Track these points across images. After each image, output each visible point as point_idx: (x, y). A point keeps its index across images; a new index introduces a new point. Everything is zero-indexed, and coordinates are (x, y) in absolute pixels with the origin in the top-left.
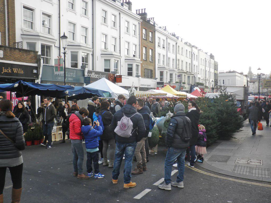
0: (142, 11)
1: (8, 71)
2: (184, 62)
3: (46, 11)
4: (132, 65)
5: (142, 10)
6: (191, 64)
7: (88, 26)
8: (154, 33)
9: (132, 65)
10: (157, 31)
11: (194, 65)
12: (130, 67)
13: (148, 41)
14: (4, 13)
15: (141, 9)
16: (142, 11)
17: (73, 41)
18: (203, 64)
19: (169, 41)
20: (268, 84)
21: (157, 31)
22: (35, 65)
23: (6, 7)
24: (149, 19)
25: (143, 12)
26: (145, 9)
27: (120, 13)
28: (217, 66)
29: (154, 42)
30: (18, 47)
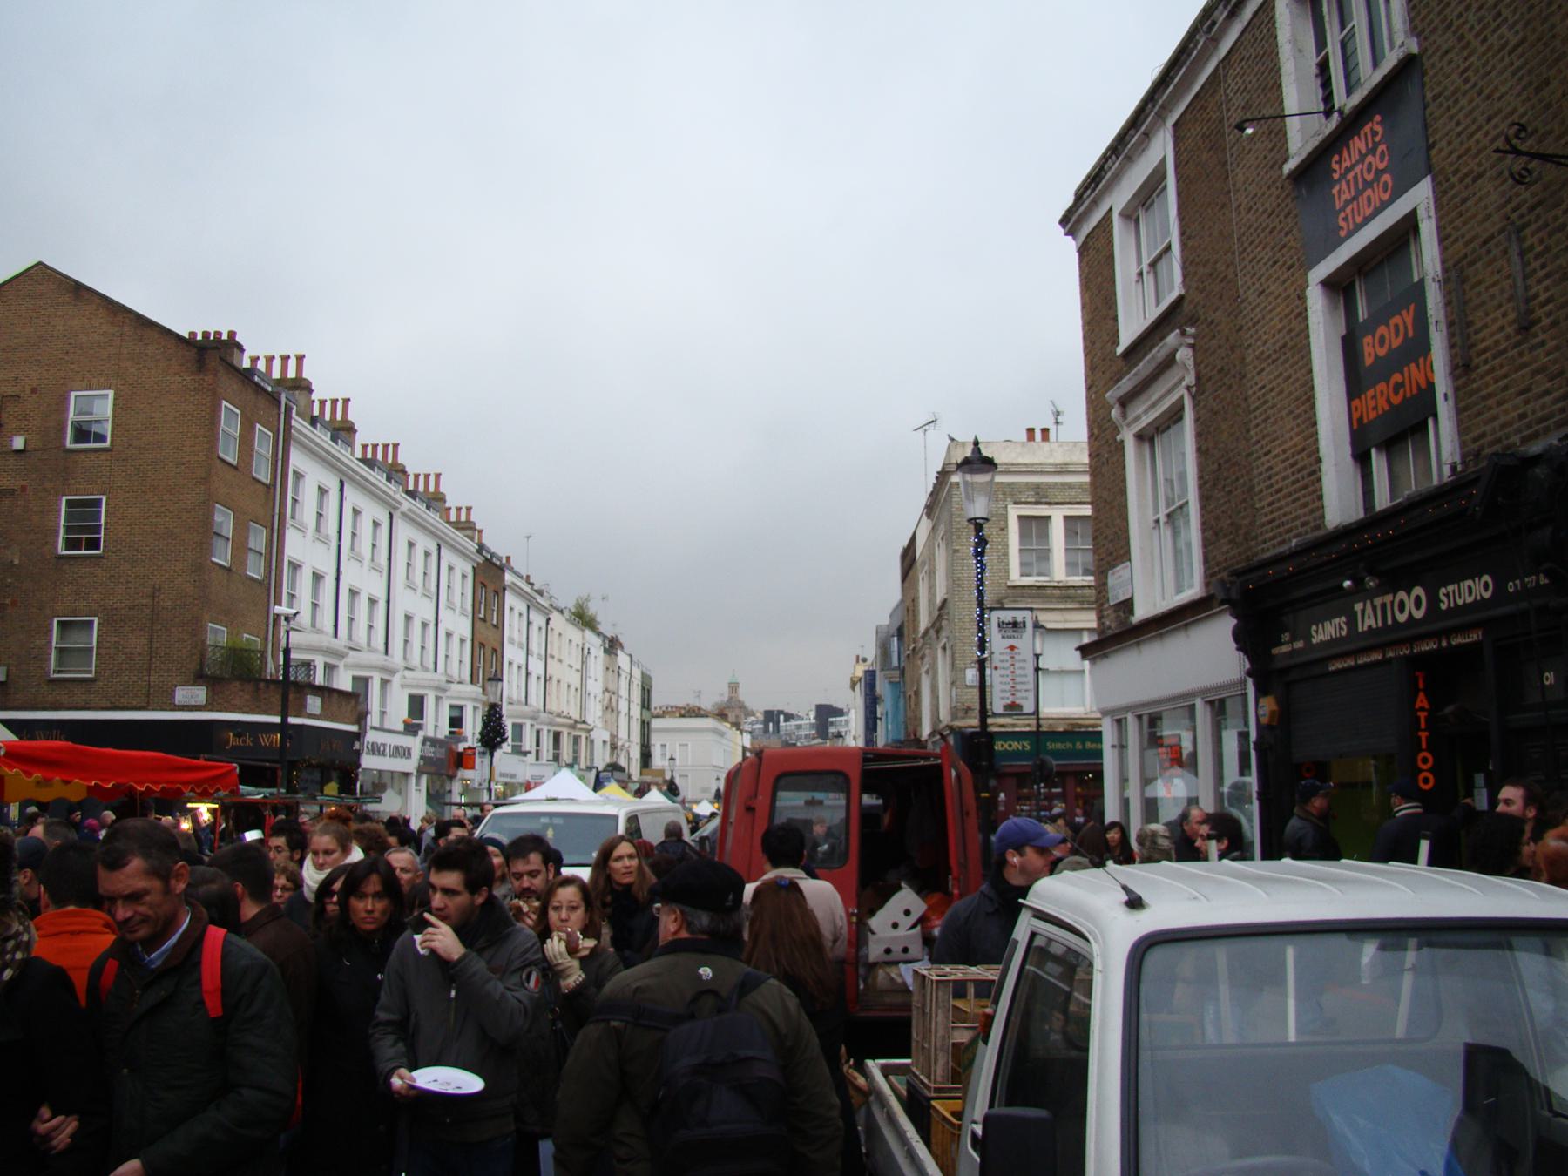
0: (459, 516)
1: (244, 741)
2: (562, 683)
3: (295, 556)
4: (461, 708)
5: (285, 359)
6: (432, 628)
7: (301, 559)
8: (501, 595)
9: (461, 708)
10: (300, 443)
11: (295, 567)
12: (456, 714)
13: (488, 623)
14: (269, 589)
15: (381, 442)
16: (459, 516)
17: (334, 640)
18: (457, 599)
19: (353, 497)
20: (1500, 316)
21: (300, 443)
22: (354, 728)
23: (273, 573)
24: (255, 360)
25: (292, 374)
26: (300, 359)
27: (439, 545)
28: (649, 691)
29: (500, 626)
30: (296, 677)
